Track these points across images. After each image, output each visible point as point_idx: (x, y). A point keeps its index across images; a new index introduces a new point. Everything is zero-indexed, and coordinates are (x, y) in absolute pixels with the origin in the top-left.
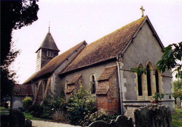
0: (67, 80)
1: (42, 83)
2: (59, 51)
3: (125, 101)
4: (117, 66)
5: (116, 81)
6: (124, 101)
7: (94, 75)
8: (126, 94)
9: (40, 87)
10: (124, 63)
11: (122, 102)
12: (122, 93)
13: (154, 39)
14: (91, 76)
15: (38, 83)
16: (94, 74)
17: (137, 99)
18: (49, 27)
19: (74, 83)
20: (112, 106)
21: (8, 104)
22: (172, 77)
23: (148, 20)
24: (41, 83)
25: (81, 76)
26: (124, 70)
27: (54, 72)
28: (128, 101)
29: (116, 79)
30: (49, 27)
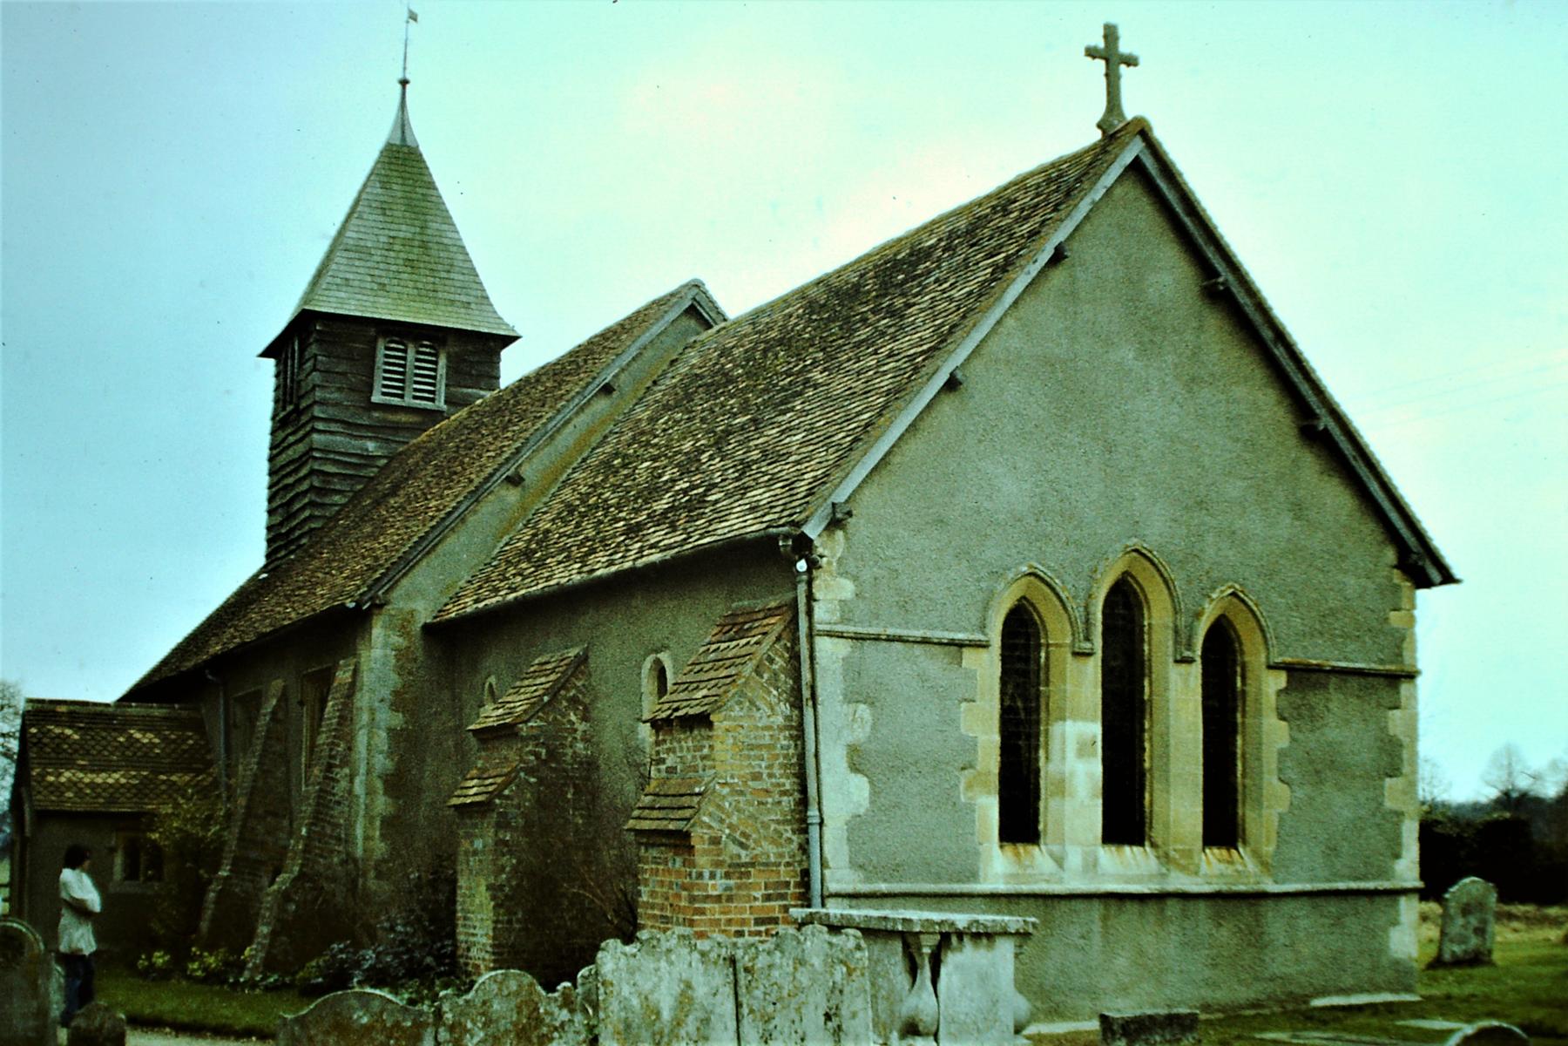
0: (492, 680)
1: (294, 700)
2: (508, 340)
3: (849, 888)
4: (795, 600)
5: (781, 729)
6: (833, 887)
7: (665, 657)
8: (856, 826)
9: (268, 737)
10: (855, 579)
11: (823, 898)
12: (821, 824)
13: (1214, 332)
14: (648, 663)
15: (256, 699)
16: (664, 648)
17: (974, 876)
18: (404, 83)
19: (511, 726)
20: (729, 922)
21: (324, 961)
22: (1411, 676)
23: (1149, 163)
24: (284, 697)
25: (582, 660)
26: (859, 638)
27: (379, 606)
28: (883, 887)
29: (784, 708)
30: (404, 83)
